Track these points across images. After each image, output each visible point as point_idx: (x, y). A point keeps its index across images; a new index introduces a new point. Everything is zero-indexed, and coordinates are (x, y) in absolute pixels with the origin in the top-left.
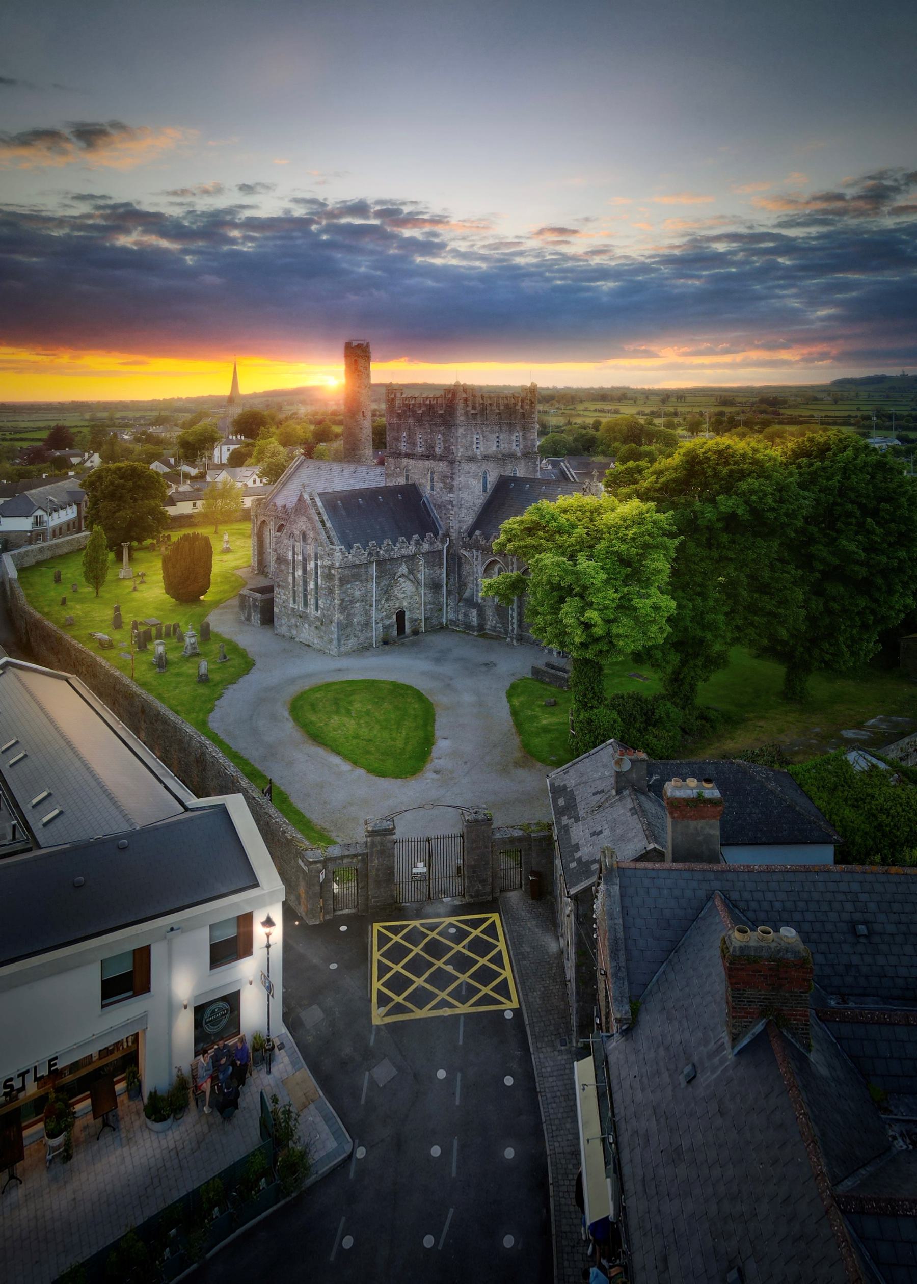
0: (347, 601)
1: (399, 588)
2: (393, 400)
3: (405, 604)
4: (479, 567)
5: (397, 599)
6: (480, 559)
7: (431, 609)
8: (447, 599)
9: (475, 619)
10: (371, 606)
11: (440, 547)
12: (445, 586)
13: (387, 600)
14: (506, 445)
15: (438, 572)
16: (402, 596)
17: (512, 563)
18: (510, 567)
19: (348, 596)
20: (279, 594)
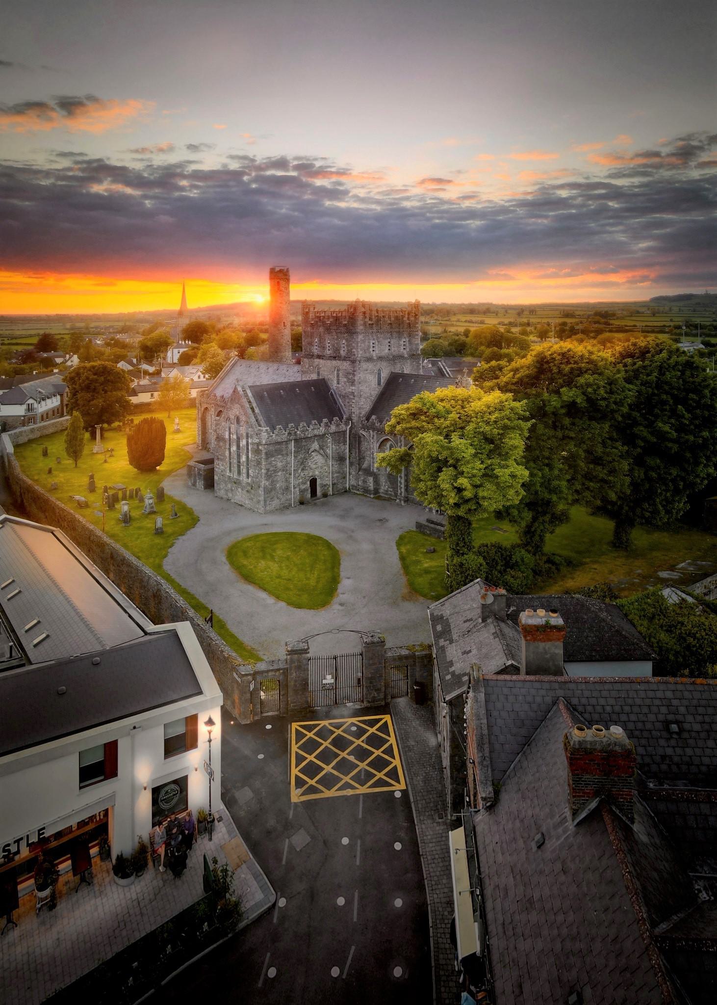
2: (307, 313)
3: (317, 473)
4: (375, 444)
5: (311, 469)
6: (375, 437)
7: (337, 477)
9: (372, 485)
10: (290, 474)
11: (344, 429)
13: (303, 470)
14: (396, 349)
15: (343, 448)
17: (401, 441)
18: (399, 444)
19: (273, 466)
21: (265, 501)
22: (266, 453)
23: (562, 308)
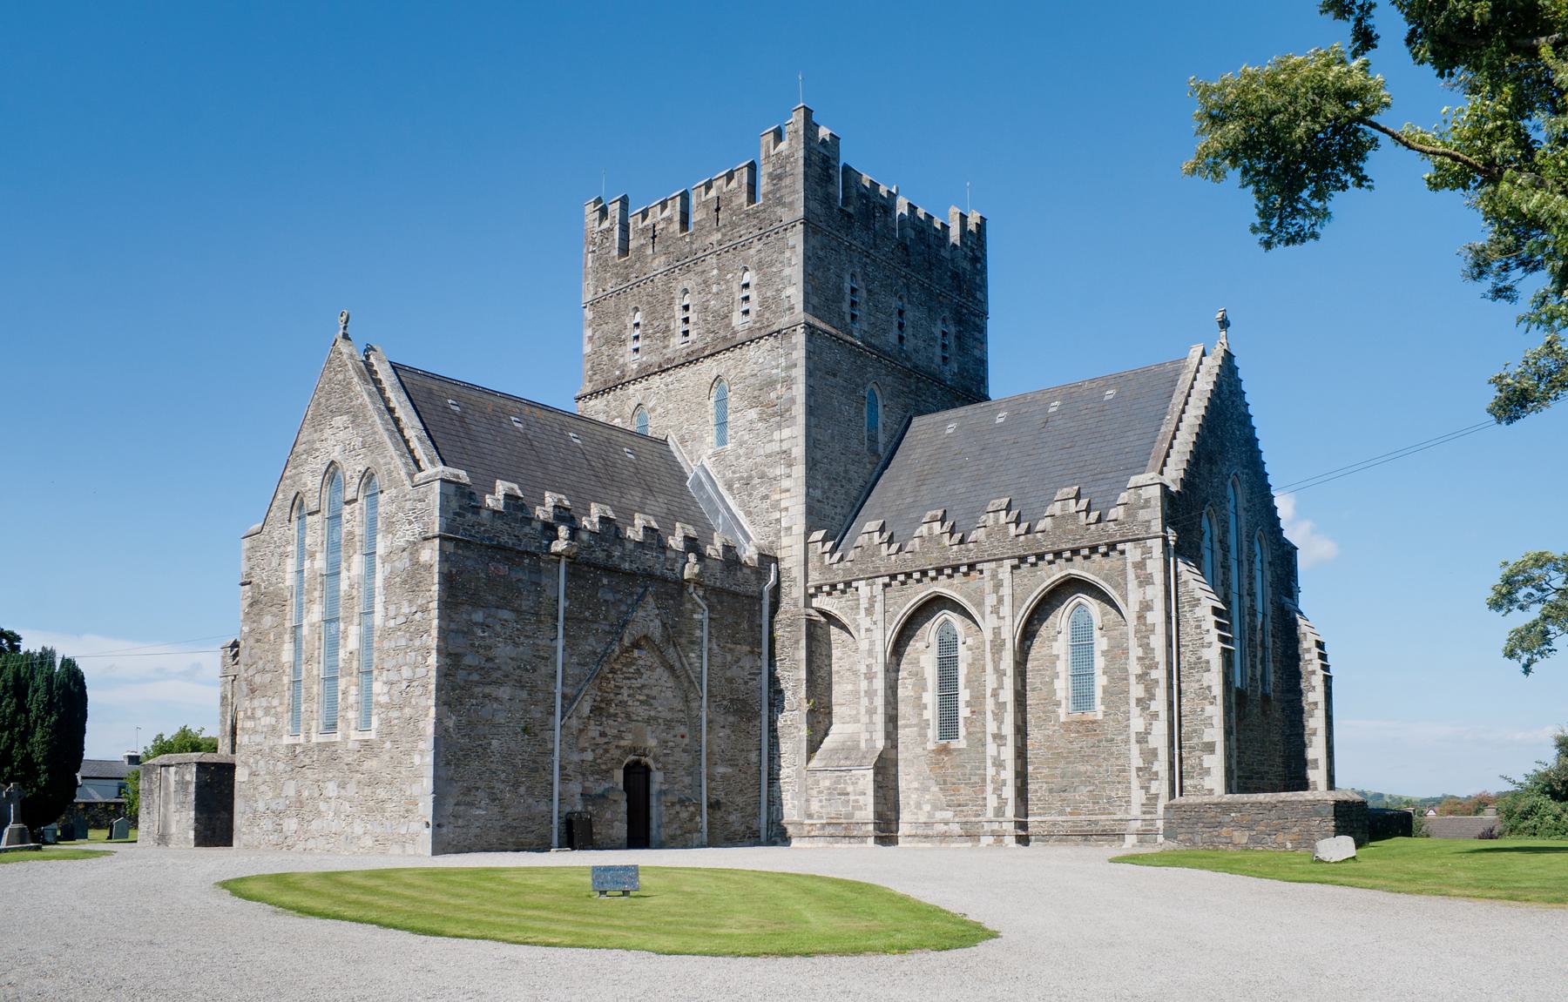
0: (471, 669)
1: (637, 683)
3: (652, 743)
5: (628, 716)
6: (879, 607)
7: (723, 776)
11: (752, 589)
13: (597, 711)
14: (921, 344)
15: (747, 663)
16: (642, 712)
17: (998, 585)
18: (991, 600)
20: (252, 717)
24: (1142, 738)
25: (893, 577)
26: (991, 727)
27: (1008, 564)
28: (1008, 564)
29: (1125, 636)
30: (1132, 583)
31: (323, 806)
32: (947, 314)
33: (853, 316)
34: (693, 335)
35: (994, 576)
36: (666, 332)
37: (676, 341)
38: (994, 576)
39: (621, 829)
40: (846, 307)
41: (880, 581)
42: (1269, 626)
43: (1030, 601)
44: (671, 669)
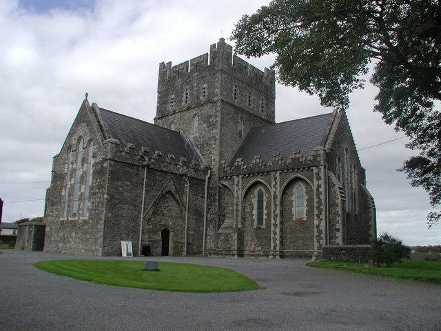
4: (240, 192)
6: (240, 184)
8: (206, 230)
12: (205, 215)
13: (154, 213)
17: (275, 179)
18: (273, 183)
21: (105, 237)
22: (112, 173)
23: (397, 271)
24: (318, 227)
25: (245, 175)
26: (273, 222)
27: (278, 172)
28: (278, 172)
29: (313, 195)
30: (315, 180)
31: (71, 240)
32: (263, 98)
33: (235, 98)
34: (188, 102)
35: (275, 175)
36: (181, 101)
37: (183, 104)
38: (275, 175)
39: (159, 250)
40: (233, 95)
41: (240, 176)
42: (357, 193)
43: (285, 184)
44: (176, 200)
